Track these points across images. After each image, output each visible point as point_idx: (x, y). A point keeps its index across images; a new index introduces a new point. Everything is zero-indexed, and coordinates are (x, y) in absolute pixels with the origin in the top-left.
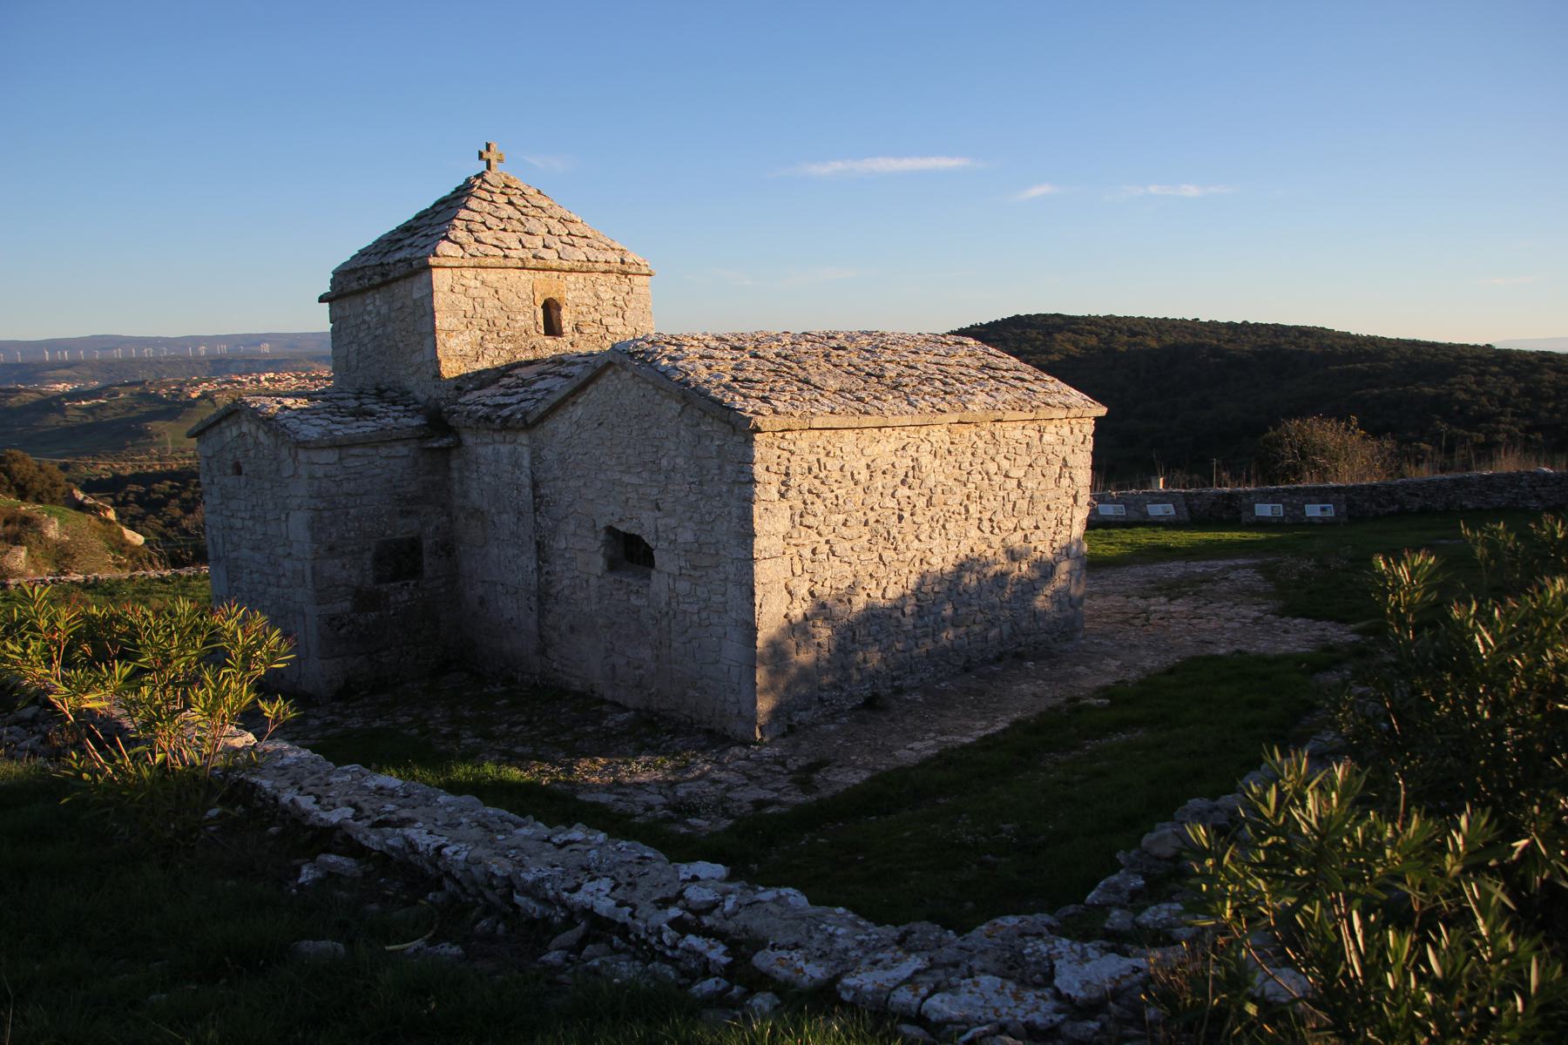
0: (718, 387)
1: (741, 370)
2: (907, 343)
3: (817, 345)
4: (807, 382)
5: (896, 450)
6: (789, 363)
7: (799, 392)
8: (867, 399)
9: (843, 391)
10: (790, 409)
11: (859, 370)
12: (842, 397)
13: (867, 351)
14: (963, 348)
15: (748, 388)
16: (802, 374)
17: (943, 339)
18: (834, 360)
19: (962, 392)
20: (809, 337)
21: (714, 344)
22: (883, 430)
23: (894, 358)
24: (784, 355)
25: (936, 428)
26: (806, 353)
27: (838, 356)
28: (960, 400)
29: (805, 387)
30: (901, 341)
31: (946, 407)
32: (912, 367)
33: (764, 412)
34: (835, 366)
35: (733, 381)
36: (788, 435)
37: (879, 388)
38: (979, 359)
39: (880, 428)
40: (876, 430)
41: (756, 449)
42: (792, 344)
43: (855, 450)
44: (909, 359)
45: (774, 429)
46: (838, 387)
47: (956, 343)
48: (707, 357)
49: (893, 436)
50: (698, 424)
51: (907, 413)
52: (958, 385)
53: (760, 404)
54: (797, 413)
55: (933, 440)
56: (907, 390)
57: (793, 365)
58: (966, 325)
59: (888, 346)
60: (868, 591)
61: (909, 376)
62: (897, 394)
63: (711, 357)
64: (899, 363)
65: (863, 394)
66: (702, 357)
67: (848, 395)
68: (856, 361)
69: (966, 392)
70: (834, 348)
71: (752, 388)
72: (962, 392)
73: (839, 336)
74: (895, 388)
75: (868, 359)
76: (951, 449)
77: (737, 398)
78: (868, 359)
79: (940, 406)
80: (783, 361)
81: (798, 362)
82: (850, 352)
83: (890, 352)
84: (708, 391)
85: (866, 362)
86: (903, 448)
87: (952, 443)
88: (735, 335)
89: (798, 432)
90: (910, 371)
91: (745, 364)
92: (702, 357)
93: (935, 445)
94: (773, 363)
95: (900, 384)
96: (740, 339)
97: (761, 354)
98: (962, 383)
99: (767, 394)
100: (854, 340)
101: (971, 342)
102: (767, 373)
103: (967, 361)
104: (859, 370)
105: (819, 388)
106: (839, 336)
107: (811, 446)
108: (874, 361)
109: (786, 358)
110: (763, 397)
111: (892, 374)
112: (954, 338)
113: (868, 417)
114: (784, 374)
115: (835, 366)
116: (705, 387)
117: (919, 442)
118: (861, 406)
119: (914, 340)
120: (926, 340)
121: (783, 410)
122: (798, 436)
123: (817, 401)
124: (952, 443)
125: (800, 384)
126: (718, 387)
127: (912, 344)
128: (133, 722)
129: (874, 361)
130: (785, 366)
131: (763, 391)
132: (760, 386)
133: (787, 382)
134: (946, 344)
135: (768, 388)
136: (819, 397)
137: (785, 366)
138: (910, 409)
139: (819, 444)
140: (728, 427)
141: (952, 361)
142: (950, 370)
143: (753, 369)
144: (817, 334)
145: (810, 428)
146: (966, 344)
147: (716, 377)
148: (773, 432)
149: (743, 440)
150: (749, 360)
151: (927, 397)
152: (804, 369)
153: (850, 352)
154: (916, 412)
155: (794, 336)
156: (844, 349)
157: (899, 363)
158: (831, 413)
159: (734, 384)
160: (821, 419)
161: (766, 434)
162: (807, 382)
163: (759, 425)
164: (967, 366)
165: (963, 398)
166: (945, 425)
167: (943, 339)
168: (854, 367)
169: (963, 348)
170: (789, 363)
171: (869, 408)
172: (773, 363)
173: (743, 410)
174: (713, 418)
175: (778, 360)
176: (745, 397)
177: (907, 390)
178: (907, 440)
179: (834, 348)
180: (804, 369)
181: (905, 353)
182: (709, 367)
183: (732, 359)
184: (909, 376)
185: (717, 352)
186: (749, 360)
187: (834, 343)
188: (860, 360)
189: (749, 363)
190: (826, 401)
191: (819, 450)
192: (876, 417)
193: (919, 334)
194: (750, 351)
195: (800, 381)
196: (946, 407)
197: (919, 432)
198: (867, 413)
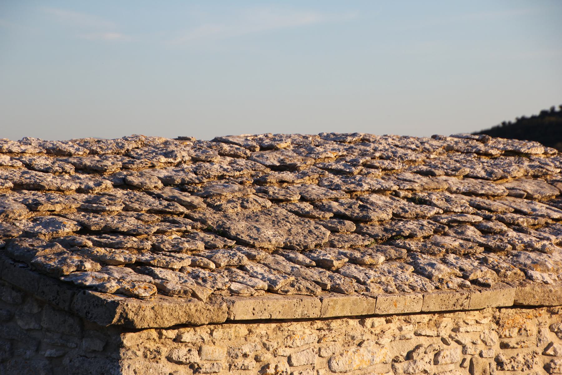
0: (50, 245)
1: (97, 211)
2: (412, 156)
3: (242, 162)
4: (223, 232)
5: (396, 360)
6: (188, 198)
7: (207, 253)
8: (336, 264)
9: (292, 248)
10: (191, 285)
11: (322, 208)
12: (290, 260)
13: (336, 172)
14: (519, 163)
15: (111, 246)
16: (213, 218)
17: (481, 147)
18: (274, 189)
19: (520, 246)
20: (226, 147)
21: (42, 161)
22: (368, 322)
23: (386, 184)
24: (178, 181)
25: (471, 318)
26: (221, 177)
27: (282, 182)
28: (515, 263)
29: (219, 242)
30: (401, 151)
31: (490, 276)
32: (422, 202)
33: (143, 294)
34: (276, 201)
35: (80, 233)
36: (188, 335)
37: (360, 241)
38: (553, 183)
39: (362, 319)
40: (354, 323)
41: (126, 363)
42: (195, 160)
43: (317, 360)
44: (416, 186)
45: (160, 323)
46: (281, 240)
47: (508, 153)
48: (29, 187)
49: (388, 334)
50: (11, 318)
51: (413, 288)
52: (512, 234)
53: (134, 276)
54: (204, 293)
55: (466, 340)
56: (413, 245)
57: (197, 200)
58: (512, 119)
59: (376, 163)
60: (317, 346)
61: (417, 217)
62: (393, 252)
63: (37, 187)
64: (397, 194)
65: (330, 255)
66: (18, 187)
67: (301, 257)
68: (315, 190)
69: (528, 247)
70: (273, 168)
71: (118, 246)
72: (520, 246)
73: (282, 145)
74: (390, 241)
75: (337, 188)
76: (503, 358)
77: (88, 265)
78: (337, 188)
79: (478, 275)
80: (176, 193)
81: (206, 196)
82: (304, 174)
83: (380, 173)
84: (32, 253)
85: (335, 194)
86: (409, 357)
87: (504, 346)
88: (84, 144)
89: (207, 329)
90: (418, 209)
91: (105, 200)
92: (18, 187)
93: (471, 350)
94: (158, 197)
95: (399, 234)
96: (93, 153)
97: (135, 180)
98: (519, 229)
99: (147, 257)
100: (311, 151)
101: (538, 150)
102: (146, 217)
103: (530, 187)
104: (322, 208)
105: (246, 244)
106: (282, 145)
107: (232, 355)
108: (349, 192)
109: (182, 187)
110: (138, 263)
111: (384, 216)
112: (502, 142)
113: (340, 298)
114: (180, 219)
115: (276, 201)
116: (26, 244)
117: (438, 344)
118: (325, 276)
119: (425, 150)
120: (449, 149)
121: (178, 287)
122: (206, 337)
123: (242, 268)
124: (504, 346)
125: (210, 237)
126: (50, 245)
127: (422, 157)
128: (368, 183)
129: (349, 192)
130: (182, 203)
131: (140, 250)
132: (133, 241)
133: (185, 234)
134: (486, 154)
135: (148, 245)
136: (246, 261)
137: (182, 203)
138: (418, 281)
139: (246, 349)
140: (71, 321)
141: (500, 188)
142: (496, 205)
143: (119, 208)
144: (241, 141)
145: (229, 321)
146: (528, 155)
147: (46, 225)
148: (159, 330)
149: (98, 345)
150: (112, 191)
151: (451, 258)
152: (218, 209)
153: (304, 174)
154: (430, 287)
155: (198, 146)
156: (293, 168)
157: (397, 194)
158: (270, 290)
159: (84, 239)
160: (251, 303)
161: (144, 334)
162: (223, 232)
163: (131, 315)
164: (530, 197)
165: (522, 259)
166: (489, 312)
167: (481, 147)
168: (312, 202)
169: (519, 163)
170: (188, 198)
171: (340, 281)
172: (158, 197)
173: (101, 288)
174: (41, 305)
175: (168, 192)
176: (104, 262)
177: (413, 245)
178: (415, 340)
179: (273, 168)
180: (218, 209)
181: (408, 175)
182: (33, 207)
183: (79, 191)
184: (417, 217)
185: (49, 178)
186: (112, 191)
187: (273, 159)
188: (322, 190)
189: (112, 198)
190: (259, 269)
191: (247, 362)
192: (354, 297)
193: (434, 137)
194: (114, 175)
195: (209, 230)
196: (490, 276)
197: (437, 325)
198: (336, 290)
